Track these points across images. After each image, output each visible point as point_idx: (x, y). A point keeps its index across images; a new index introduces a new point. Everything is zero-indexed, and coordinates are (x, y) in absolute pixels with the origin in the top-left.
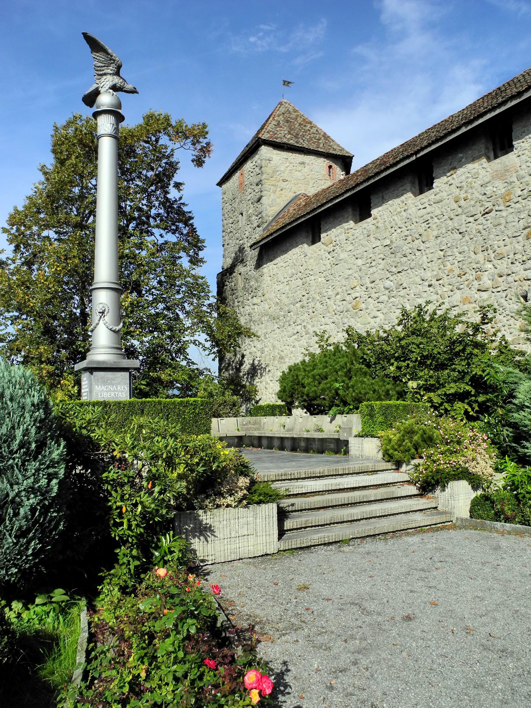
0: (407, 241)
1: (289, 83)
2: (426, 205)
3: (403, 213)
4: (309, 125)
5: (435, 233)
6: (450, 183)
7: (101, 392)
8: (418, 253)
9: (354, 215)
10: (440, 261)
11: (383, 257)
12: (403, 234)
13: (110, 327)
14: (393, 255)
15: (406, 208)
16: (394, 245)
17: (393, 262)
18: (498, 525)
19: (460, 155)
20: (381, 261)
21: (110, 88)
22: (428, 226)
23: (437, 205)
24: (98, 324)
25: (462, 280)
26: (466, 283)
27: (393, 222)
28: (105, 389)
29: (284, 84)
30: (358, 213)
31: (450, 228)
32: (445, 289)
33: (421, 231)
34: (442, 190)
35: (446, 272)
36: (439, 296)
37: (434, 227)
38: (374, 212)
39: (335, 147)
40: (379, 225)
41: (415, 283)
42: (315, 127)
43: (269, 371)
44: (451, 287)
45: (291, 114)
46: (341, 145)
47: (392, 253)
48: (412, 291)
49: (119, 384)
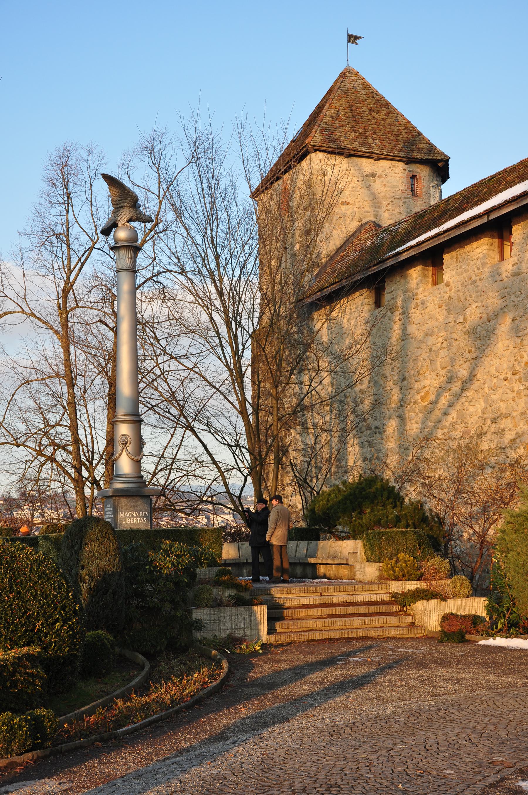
1: (357, 38)
7: (124, 518)
13: (133, 457)
22: (505, 304)
24: (121, 454)
28: (128, 515)
29: (349, 41)
36: (515, 394)
43: (440, 306)
49: (141, 511)
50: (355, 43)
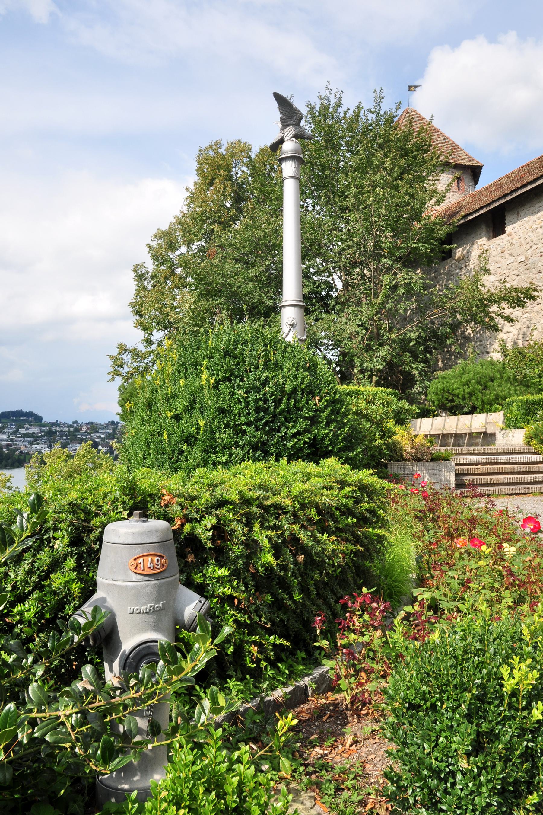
1: (415, 87)
3: (539, 230)
4: (436, 134)
9: (488, 232)
11: (518, 273)
12: (538, 251)
16: (530, 261)
17: (528, 278)
20: (515, 277)
21: (293, 137)
24: (288, 334)
27: (529, 239)
29: (409, 90)
30: (492, 229)
38: (508, 229)
39: (464, 157)
40: (514, 241)
42: (443, 135)
45: (417, 122)
47: (527, 270)
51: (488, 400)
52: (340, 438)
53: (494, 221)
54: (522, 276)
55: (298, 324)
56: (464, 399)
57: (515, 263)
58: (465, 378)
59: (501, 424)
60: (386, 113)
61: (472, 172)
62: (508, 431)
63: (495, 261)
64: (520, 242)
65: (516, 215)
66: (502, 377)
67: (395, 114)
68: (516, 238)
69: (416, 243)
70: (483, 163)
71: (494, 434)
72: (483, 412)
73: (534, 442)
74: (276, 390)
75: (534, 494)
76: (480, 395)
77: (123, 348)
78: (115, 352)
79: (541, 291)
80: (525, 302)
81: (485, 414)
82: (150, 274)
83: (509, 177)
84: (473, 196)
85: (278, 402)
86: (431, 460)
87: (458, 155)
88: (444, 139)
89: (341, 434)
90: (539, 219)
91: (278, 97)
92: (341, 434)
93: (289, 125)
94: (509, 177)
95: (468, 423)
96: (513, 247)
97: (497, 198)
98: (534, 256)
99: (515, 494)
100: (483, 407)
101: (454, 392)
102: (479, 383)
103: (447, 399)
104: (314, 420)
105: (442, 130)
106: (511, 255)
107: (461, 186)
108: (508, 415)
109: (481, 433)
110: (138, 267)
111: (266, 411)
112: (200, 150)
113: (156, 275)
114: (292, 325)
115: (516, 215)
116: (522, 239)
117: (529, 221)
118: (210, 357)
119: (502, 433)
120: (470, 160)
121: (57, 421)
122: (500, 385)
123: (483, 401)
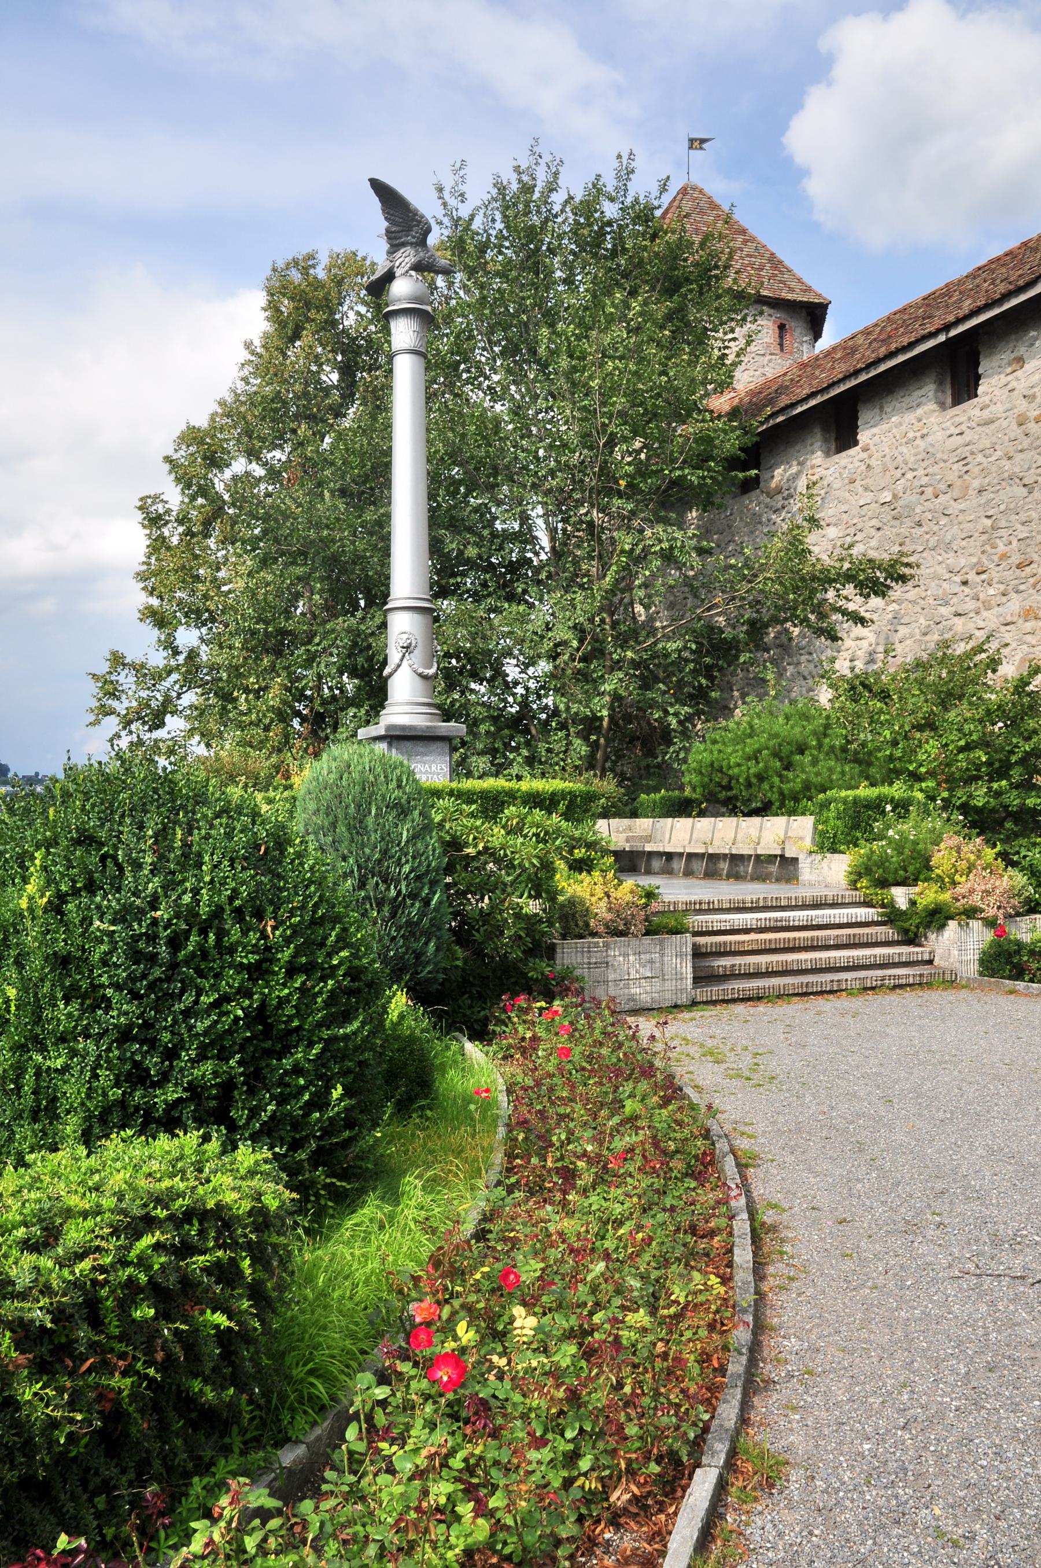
0: (924, 497)
1: (703, 141)
2: (963, 427)
3: (919, 442)
5: (976, 484)
6: (1010, 387)
8: (943, 521)
9: (826, 440)
10: (985, 537)
12: (916, 483)
14: (897, 523)
15: (925, 431)
16: (901, 503)
17: (898, 535)
18: (1020, 985)
19: (1033, 333)
20: (873, 532)
21: (411, 269)
22: (966, 469)
23: (983, 428)
24: (399, 666)
25: (1023, 574)
26: (1032, 580)
27: (900, 459)
29: (691, 148)
30: (833, 435)
31: (1006, 475)
32: (991, 591)
33: (952, 477)
34: (995, 400)
35: (996, 558)
36: (979, 604)
37: (976, 470)
39: (793, 284)
40: (873, 462)
41: (937, 577)
42: (753, 239)
44: (1002, 587)
46: (805, 280)
47: (895, 518)
48: (929, 593)
50: (701, 148)
51: (791, 790)
52: (319, 1000)
53: (837, 420)
54: (887, 531)
55: (419, 645)
56: (749, 785)
57: (874, 505)
58: (751, 745)
59: (808, 843)
60: (636, 201)
61: (808, 314)
62: (819, 857)
63: (837, 499)
64: (884, 465)
65: (877, 410)
66: (820, 745)
67: (656, 203)
68: (876, 455)
69: (679, 468)
70: (830, 298)
71: (795, 860)
72: (783, 814)
73: (864, 882)
74: (177, 916)
75: (850, 992)
76: (776, 780)
77: (117, 660)
78: (103, 668)
79: (918, 566)
80: (889, 587)
81: (784, 819)
82: (174, 513)
83: (869, 333)
84: (803, 366)
85: (176, 943)
86: (648, 933)
87: (781, 282)
88: (756, 248)
89: (320, 992)
90: (920, 420)
91: (380, 188)
92: (320, 992)
93: (403, 245)
94: (869, 333)
95: (754, 833)
96: (870, 473)
97: (840, 376)
98: (908, 492)
99: (812, 993)
100: (782, 805)
101: (731, 772)
102: (776, 755)
103: (719, 785)
104: (258, 971)
105: (753, 230)
106: (866, 489)
107: (786, 343)
108: (820, 827)
109: (776, 856)
110: (149, 501)
111: (153, 958)
112: (274, 270)
113: (185, 517)
114: (407, 648)
115: (877, 410)
116: (887, 459)
117: (901, 424)
118: (49, 844)
119: (809, 860)
120: (805, 291)
121: (37, 774)
122: (815, 762)
123: (781, 793)
